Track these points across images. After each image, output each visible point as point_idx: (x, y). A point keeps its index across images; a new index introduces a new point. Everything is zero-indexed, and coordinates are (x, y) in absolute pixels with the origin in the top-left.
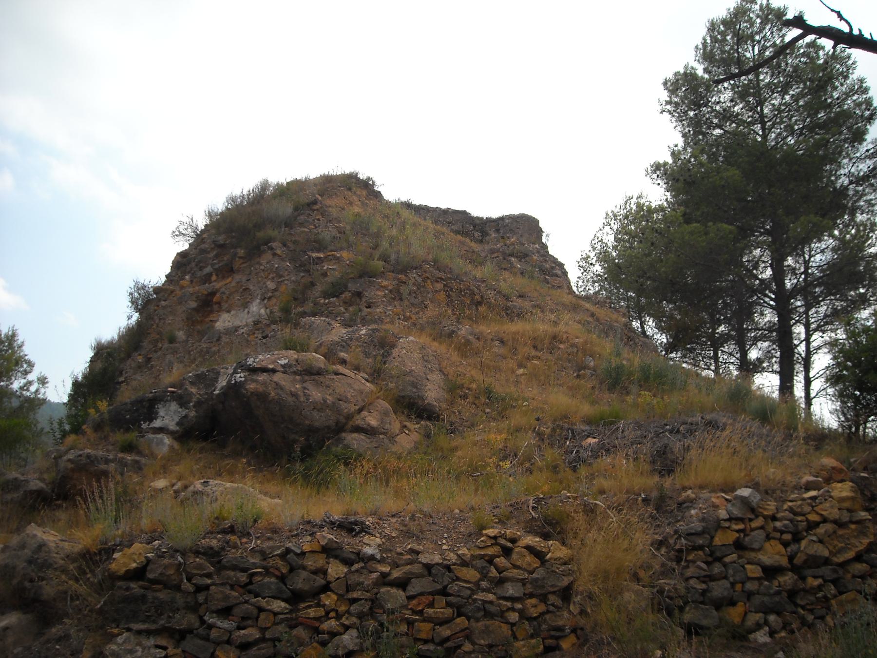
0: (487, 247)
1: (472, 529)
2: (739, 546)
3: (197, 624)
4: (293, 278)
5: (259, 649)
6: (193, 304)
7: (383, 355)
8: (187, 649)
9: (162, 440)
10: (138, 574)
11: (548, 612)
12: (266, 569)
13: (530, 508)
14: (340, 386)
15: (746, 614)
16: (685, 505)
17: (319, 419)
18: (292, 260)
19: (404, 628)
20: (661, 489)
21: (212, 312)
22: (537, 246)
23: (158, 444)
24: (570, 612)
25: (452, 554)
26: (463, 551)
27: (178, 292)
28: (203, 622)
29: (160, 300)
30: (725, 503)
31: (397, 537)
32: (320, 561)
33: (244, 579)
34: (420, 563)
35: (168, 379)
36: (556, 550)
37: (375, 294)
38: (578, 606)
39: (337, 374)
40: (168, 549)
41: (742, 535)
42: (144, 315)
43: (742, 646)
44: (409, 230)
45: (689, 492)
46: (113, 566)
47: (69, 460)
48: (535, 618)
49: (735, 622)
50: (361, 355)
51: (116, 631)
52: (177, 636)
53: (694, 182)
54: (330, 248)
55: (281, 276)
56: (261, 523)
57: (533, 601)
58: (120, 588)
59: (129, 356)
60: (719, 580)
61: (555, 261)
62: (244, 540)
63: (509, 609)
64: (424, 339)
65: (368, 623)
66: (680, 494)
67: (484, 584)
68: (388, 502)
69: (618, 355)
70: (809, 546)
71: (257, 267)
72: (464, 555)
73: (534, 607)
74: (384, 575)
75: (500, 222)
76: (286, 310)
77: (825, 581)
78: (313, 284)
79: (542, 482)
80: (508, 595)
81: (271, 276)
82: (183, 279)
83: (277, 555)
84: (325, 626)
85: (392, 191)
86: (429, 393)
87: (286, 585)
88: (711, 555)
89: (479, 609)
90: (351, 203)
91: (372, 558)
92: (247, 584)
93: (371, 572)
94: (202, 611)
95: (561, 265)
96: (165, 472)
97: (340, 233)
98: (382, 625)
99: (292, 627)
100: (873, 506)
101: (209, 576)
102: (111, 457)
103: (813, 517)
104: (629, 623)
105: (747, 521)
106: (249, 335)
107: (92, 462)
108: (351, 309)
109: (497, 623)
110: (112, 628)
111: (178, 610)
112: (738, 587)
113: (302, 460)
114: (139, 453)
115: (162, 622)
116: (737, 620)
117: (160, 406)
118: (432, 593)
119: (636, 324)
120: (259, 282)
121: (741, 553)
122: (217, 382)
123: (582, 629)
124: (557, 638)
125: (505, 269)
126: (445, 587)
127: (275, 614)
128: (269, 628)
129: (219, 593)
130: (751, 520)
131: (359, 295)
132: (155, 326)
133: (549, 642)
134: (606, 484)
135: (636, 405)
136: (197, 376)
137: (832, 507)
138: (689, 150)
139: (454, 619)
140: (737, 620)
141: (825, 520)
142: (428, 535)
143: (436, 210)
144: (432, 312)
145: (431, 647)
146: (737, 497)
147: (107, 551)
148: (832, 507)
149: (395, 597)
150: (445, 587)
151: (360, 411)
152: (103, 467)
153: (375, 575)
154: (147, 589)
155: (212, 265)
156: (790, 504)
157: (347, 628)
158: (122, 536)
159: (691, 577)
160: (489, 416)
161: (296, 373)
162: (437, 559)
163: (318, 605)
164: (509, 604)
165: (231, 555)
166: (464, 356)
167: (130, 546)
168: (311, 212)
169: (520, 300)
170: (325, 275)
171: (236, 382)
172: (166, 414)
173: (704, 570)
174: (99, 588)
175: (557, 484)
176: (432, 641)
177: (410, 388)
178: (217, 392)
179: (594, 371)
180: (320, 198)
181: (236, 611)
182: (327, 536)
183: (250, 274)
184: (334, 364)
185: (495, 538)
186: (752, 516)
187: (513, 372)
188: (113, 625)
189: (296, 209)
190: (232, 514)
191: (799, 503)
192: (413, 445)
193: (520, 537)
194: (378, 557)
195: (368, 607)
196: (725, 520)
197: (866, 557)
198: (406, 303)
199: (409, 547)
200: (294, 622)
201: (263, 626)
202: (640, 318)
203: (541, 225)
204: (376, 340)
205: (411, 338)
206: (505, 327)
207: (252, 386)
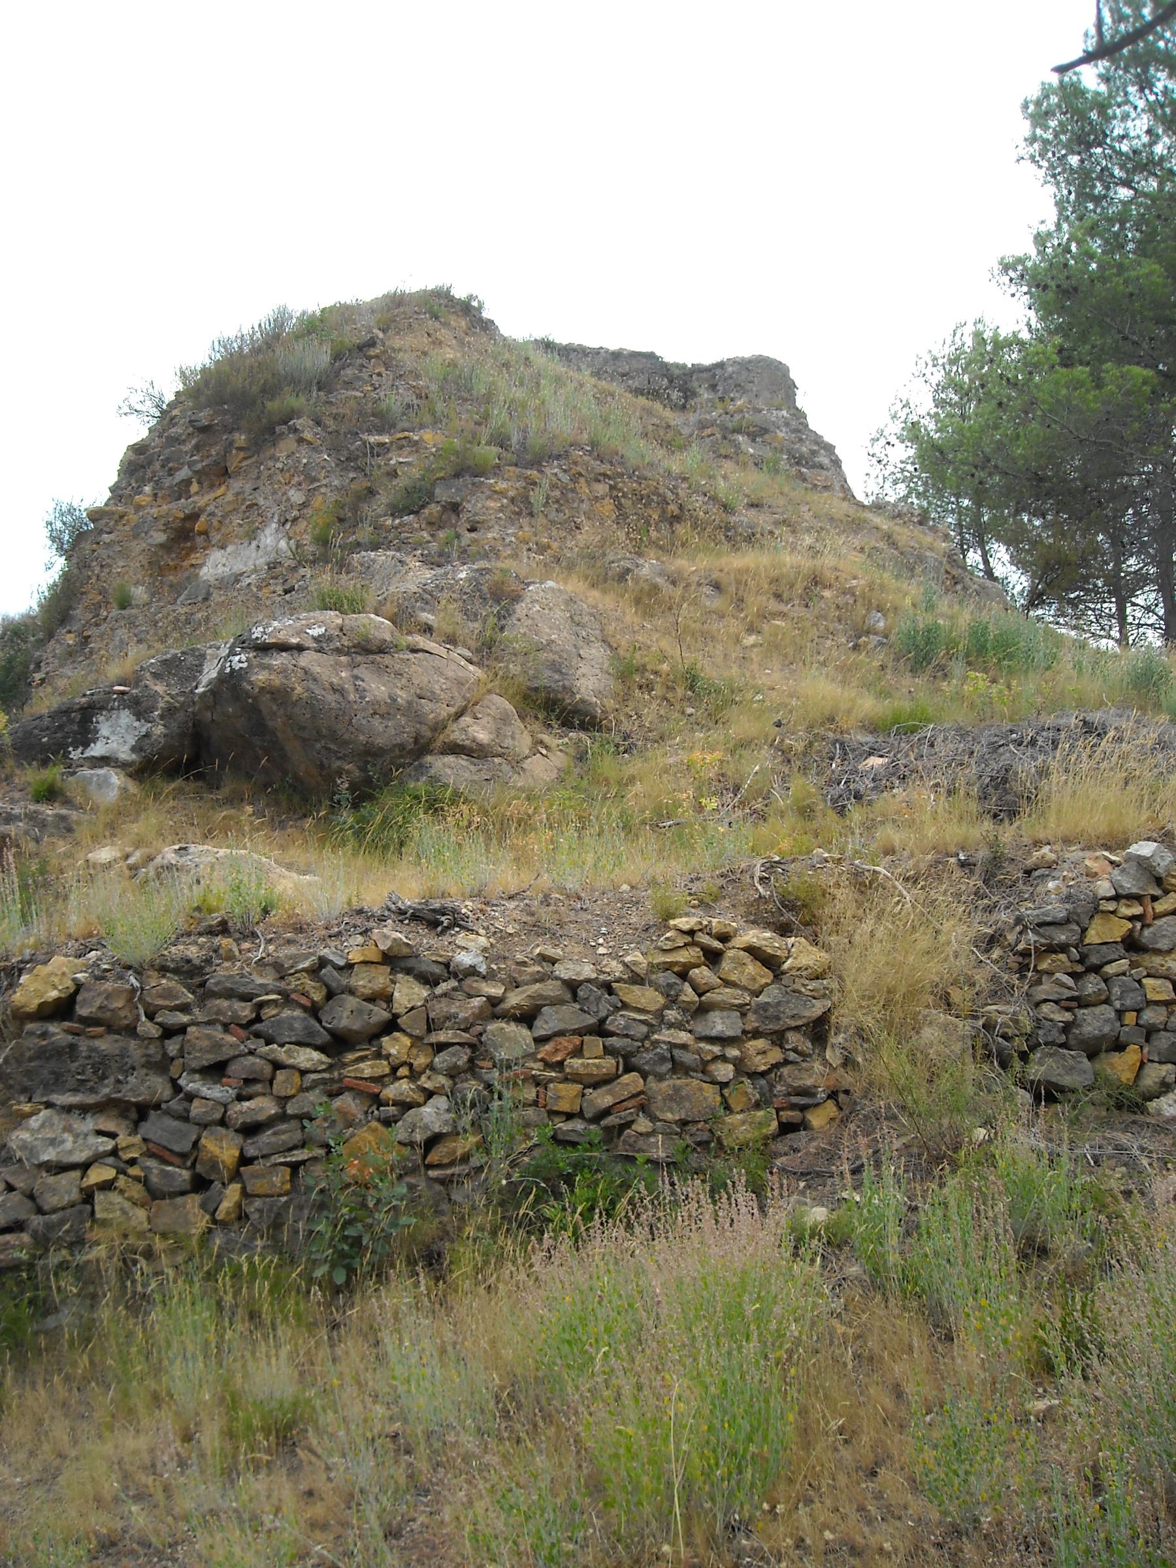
0: (693, 418)
1: (651, 919)
2: (1132, 944)
3: (167, 1092)
4: (336, 483)
5: (275, 1134)
6: (160, 537)
7: (499, 616)
8: (150, 1136)
10: (63, 1009)
11: (787, 1062)
12: (285, 995)
13: (756, 880)
14: (420, 672)
15: (1142, 1064)
16: (1037, 873)
17: (384, 733)
18: (334, 449)
20: (994, 844)
21: (193, 549)
22: (784, 413)
23: (100, 786)
24: (825, 1062)
25: (614, 963)
27: (133, 518)
28: (177, 1089)
29: (101, 532)
30: (1109, 868)
31: (517, 934)
32: (379, 979)
33: (246, 1012)
34: (557, 978)
35: (114, 670)
36: (801, 954)
37: (480, 505)
38: (838, 1052)
39: (415, 651)
40: (113, 964)
41: (1138, 925)
42: (75, 560)
43: (1134, 1122)
44: (546, 392)
45: (1046, 850)
46: (18, 997)
48: (763, 1074)
49: (1124, 1080)
50: (459, 617)
51: (27, 1108)
52: (134, 1115)
53: (1076, 289)
54: (400, 425)
55: (315, 480)
56: (275, 917)
57: (761, 1043)
58: (31, 1033)
59: (51, 635)
60: (1094, 1005)
61: (818, 440)
62: (246, 945)
64: (575, 585)
65: (465, 1085)
66: (1029, 853)
68: (503, 874)
69: (930, 607)
71: (271, 464)
72: (635, 963)
73: (760, 1054)
74: (494, 1002)
76: (323, 541)
78: (371, 492)
79: (782, 835)
80: (714, 1033)
81: (296, 479)
83: (303, 970)
85: (517, 319)
86: (582, 681)
87: (320, 1022)
89: (663, 1059)
90: (438, 343)
91: (472, 971)
92: (251, 1022)
93: (470, 996)
94: (174, 1070)
95: (830, 449)
96: (113, 835)
97: (419, 397)
98: (489, 1086)
99: (332, 1095)
101: (185, 1008)
102: (17, 811)
104: (930, 1081)
105: (1148, 900)
106: (259, 588)
108: (441, 534)
109: (695, 1082)
110: (19, 1103)
111: (134, 1069)
112: (1130, 1018)
113: (356, 806)
114: (67, 802)
115: (106, 1091)
116: (1127, 1076)
117: (101, 718)
118: (579, 1032)
119: (974, 557)
120: (275, 493)
122: (201, 672)
123: (847, 1092)
124: (803, 1108)
125: (726, 457)
126: (602, 1021)
127: (303, 1073)
128: (293, 1096)
130: (1155, 899)
131: (455, 508)
132: (93, 580)
133: (787, 1115)
134: (896, 837)
135: (959, 697)
138: (1065, 226)
139: (618, 1077)
140: (1127, 1076)
142: (572, 929)
143: (597, 352)
144: (588, 535)
145: (579, 1125)
146: (1129, 858)
149: (511, 1040)
150: (602, 1021)
153: (477, 1002)
154: (77, 1034)
157: (429, 1094)
158: (35, 947)
159: (1046, 1001)
160: (692, 719)
161: (339, 651)
163: (378, 1055)
164: (716, 1049)
165: (223, 973)
166: (648, 613)
167: (45, 963)
168: (365, 362)
169: (753, 512)
170: (393, 474)
171: (233, 670)
172: (113, 733)
173: (1069, 988)
175: (810, 836)
176: (580, 1115)
177: (548, 673)
178: (200, 690)
179: (886, 637)
180: (381, 335)
181: (233, 1068)
182: (391, 934)
183: (258, 478)
184: (409, 633)
185: (691, 933)
186: (1157, 892)
187: (738, 640)
188: (22, 1098)
189: (337, 357)
190: (225, 904)
192: (554, 776)
193: (736, 930)
194: (483, 969)
195: (465, 1058)
196: (1108, 899)
198: (541, 520)
199: (537, 951)
200: (336, 1086)
201: (283, 1094)
202: (982, 544)
203: (792, 375)
204: (485, 589)
206: (724, 560)
207: (260, 677)
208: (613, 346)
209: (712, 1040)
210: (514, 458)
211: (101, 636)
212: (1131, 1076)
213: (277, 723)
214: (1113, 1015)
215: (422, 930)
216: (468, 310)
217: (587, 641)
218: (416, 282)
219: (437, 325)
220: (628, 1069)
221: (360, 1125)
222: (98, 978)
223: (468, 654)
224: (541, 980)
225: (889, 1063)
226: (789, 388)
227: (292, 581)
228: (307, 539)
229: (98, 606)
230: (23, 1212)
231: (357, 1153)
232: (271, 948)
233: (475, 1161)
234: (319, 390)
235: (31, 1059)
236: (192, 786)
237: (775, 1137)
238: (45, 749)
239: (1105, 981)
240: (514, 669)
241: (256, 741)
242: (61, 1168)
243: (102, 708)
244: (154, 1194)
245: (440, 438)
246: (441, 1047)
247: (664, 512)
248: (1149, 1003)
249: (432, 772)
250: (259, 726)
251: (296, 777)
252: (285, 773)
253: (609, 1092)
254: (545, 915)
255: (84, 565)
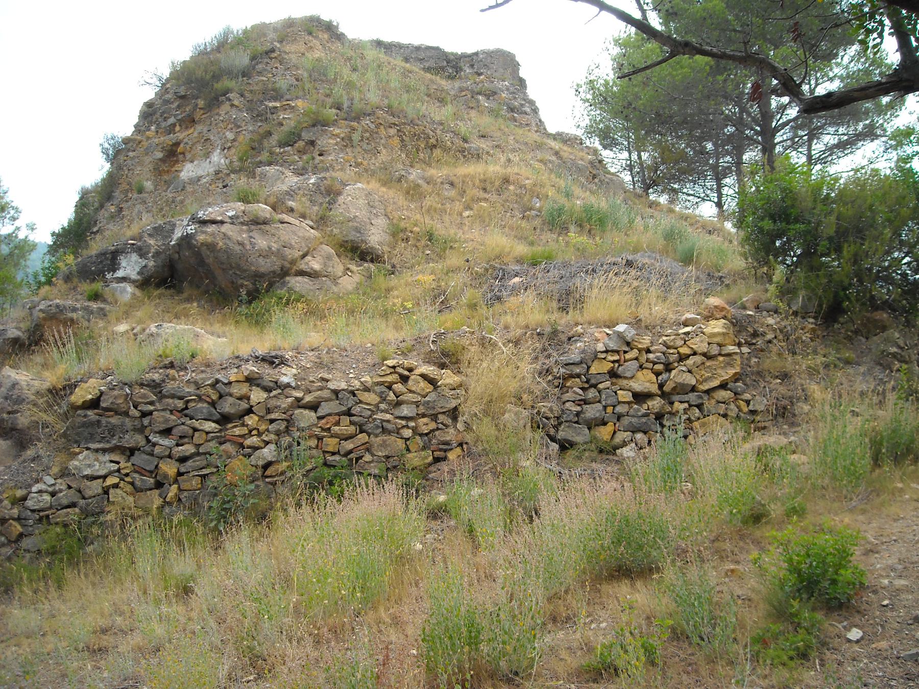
0: (457, 84)
1: (377, 361)
2: (613, 374)
6: (160, 155)
7: (329, 203)
9: (125, 289)
10: (94, 404)
11: (438, 429)
14: (284, 234)
15: (615, 432)
17: (265, 265)
18: (249, 110)
19: (313, 443)
21: (177, 162)
23: (121, 293)
26: (367, 378)
28: (148, 441)
29: (129, 150)
31: (311, 368)
32: (244, 389)
36: (448, 378)
37: (326, 142)
41: (617, 365)
46: (73, 398)
47: (41, 310)
48: (427, 434)
51: (77, 450)
52: (128, 453)
55: (239, 127)
57: (425, 420)
59: (102, 206)
62: (182, 373)
63: (403, 427)
64: (374, 185)
67: (382, 406)
68: (315, 338)
70: (679, 376)
71: (217, 117)
72: (366, 382)
73: (425, 425)
74: (298, 400)
75: (475, 57)
77: (690, 406)
78: (269, 134)
80: (403, 415)
81: (230, 126)
82: (149, 130)
84: (248, 442)
88: (587, 382)
89: (378, 427)
91: (288, 385)
92: (183, 410)
93: (287, 397)
94: (147, 432)
97: (297, 80)
99: (221, 444)
100: (754, 341)
103: (684, 350)
107: (62, 311)
108: (305, 157)
112: (609, 410)
114: (104, 301)
115: (114, 442)
116: (607, 437)
118: (339, 414)
120: (219, 133)
121: (614, 380)
123: (466, 443)
124: (445, 451)
126: (350, 409)
127: (207, 433)
129: (161, 418)
130: (625, 352)
131: (312, 143)
133: (437, 454)
136: (155, 228)
137: (702, 341)
141: (695, 354)
142: (339, 365)
143: (407, 47)
144: (384, 156)
145: (337, 458)
146: (615, 332)
147: (71, 387)
148: (702, 341)
149: (306, 417)
150: (350, 409)
151: (304, 256)
152: (70, 315)
153: (290, 400)
155: (175, 116)
156: (665, 338)
157: (267, 443)
161: (242, 224)
162: (343, 385)
163: (243, 425)
164: (404, 423)
165: (170, 386)
168: (269, 60)
174: (65, 416)
176: (338, 453)
177: (354, 233)
178: (173, 243)
179: (539, 211)
180: (278, 45)
181: (174, 431)
182: (251, 368)
185: (394, 367)
186: (627, 349)
189: (253, 58)
191: (672, 337)
193: (416, 366)
194: (293, 384)
196: (602, 352)
197: (731, 385)
203: (517, 59)
204: (322, 188)
205: (359, 185)
207: (201, 238)
208: (416, 43)
209: (402, 418)
210: (345, 116)
211: (128, 208)
212: (609, 437)
213: (210, 260)
214: (601, 408)
215: (266, 366)
216: (329, 28)
217: (376, 215)
218: (299, 12)
219: (311, 38)
220: (361, 432)
221: (234, 457)
222: (111, 389)
223: (311, 223)
224: (321, 390)
225: (486, 429)
226: (515, 66)
227: (227, 182)
228: (235, 158)
229: (127, 191)
230: (76, 498)
231: (233, 471)
232: (194, 374)
233: (289, 474)
234: (243, 76)
235: (79, 428)
236: (168, 292)
237: (430, 464)
238: (93, 273)
239: (599, 392)
240: (336, 231)
241: (200, 269)
242: (93, 478)
243: (122, 252)
244: (137, 490)
245: (306, 105)
246: (272, 421)
247: (427, 143)
248: (619, 403)
249: (289, 285)
250: (202, 262)
251: (220, 287)
252: (215, 286)
253: (352, 443)
254: (326, 359)
255: (120, 168)
